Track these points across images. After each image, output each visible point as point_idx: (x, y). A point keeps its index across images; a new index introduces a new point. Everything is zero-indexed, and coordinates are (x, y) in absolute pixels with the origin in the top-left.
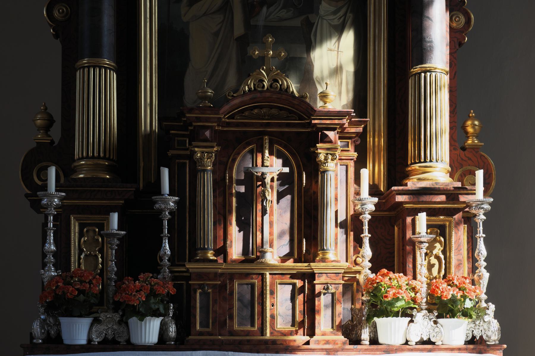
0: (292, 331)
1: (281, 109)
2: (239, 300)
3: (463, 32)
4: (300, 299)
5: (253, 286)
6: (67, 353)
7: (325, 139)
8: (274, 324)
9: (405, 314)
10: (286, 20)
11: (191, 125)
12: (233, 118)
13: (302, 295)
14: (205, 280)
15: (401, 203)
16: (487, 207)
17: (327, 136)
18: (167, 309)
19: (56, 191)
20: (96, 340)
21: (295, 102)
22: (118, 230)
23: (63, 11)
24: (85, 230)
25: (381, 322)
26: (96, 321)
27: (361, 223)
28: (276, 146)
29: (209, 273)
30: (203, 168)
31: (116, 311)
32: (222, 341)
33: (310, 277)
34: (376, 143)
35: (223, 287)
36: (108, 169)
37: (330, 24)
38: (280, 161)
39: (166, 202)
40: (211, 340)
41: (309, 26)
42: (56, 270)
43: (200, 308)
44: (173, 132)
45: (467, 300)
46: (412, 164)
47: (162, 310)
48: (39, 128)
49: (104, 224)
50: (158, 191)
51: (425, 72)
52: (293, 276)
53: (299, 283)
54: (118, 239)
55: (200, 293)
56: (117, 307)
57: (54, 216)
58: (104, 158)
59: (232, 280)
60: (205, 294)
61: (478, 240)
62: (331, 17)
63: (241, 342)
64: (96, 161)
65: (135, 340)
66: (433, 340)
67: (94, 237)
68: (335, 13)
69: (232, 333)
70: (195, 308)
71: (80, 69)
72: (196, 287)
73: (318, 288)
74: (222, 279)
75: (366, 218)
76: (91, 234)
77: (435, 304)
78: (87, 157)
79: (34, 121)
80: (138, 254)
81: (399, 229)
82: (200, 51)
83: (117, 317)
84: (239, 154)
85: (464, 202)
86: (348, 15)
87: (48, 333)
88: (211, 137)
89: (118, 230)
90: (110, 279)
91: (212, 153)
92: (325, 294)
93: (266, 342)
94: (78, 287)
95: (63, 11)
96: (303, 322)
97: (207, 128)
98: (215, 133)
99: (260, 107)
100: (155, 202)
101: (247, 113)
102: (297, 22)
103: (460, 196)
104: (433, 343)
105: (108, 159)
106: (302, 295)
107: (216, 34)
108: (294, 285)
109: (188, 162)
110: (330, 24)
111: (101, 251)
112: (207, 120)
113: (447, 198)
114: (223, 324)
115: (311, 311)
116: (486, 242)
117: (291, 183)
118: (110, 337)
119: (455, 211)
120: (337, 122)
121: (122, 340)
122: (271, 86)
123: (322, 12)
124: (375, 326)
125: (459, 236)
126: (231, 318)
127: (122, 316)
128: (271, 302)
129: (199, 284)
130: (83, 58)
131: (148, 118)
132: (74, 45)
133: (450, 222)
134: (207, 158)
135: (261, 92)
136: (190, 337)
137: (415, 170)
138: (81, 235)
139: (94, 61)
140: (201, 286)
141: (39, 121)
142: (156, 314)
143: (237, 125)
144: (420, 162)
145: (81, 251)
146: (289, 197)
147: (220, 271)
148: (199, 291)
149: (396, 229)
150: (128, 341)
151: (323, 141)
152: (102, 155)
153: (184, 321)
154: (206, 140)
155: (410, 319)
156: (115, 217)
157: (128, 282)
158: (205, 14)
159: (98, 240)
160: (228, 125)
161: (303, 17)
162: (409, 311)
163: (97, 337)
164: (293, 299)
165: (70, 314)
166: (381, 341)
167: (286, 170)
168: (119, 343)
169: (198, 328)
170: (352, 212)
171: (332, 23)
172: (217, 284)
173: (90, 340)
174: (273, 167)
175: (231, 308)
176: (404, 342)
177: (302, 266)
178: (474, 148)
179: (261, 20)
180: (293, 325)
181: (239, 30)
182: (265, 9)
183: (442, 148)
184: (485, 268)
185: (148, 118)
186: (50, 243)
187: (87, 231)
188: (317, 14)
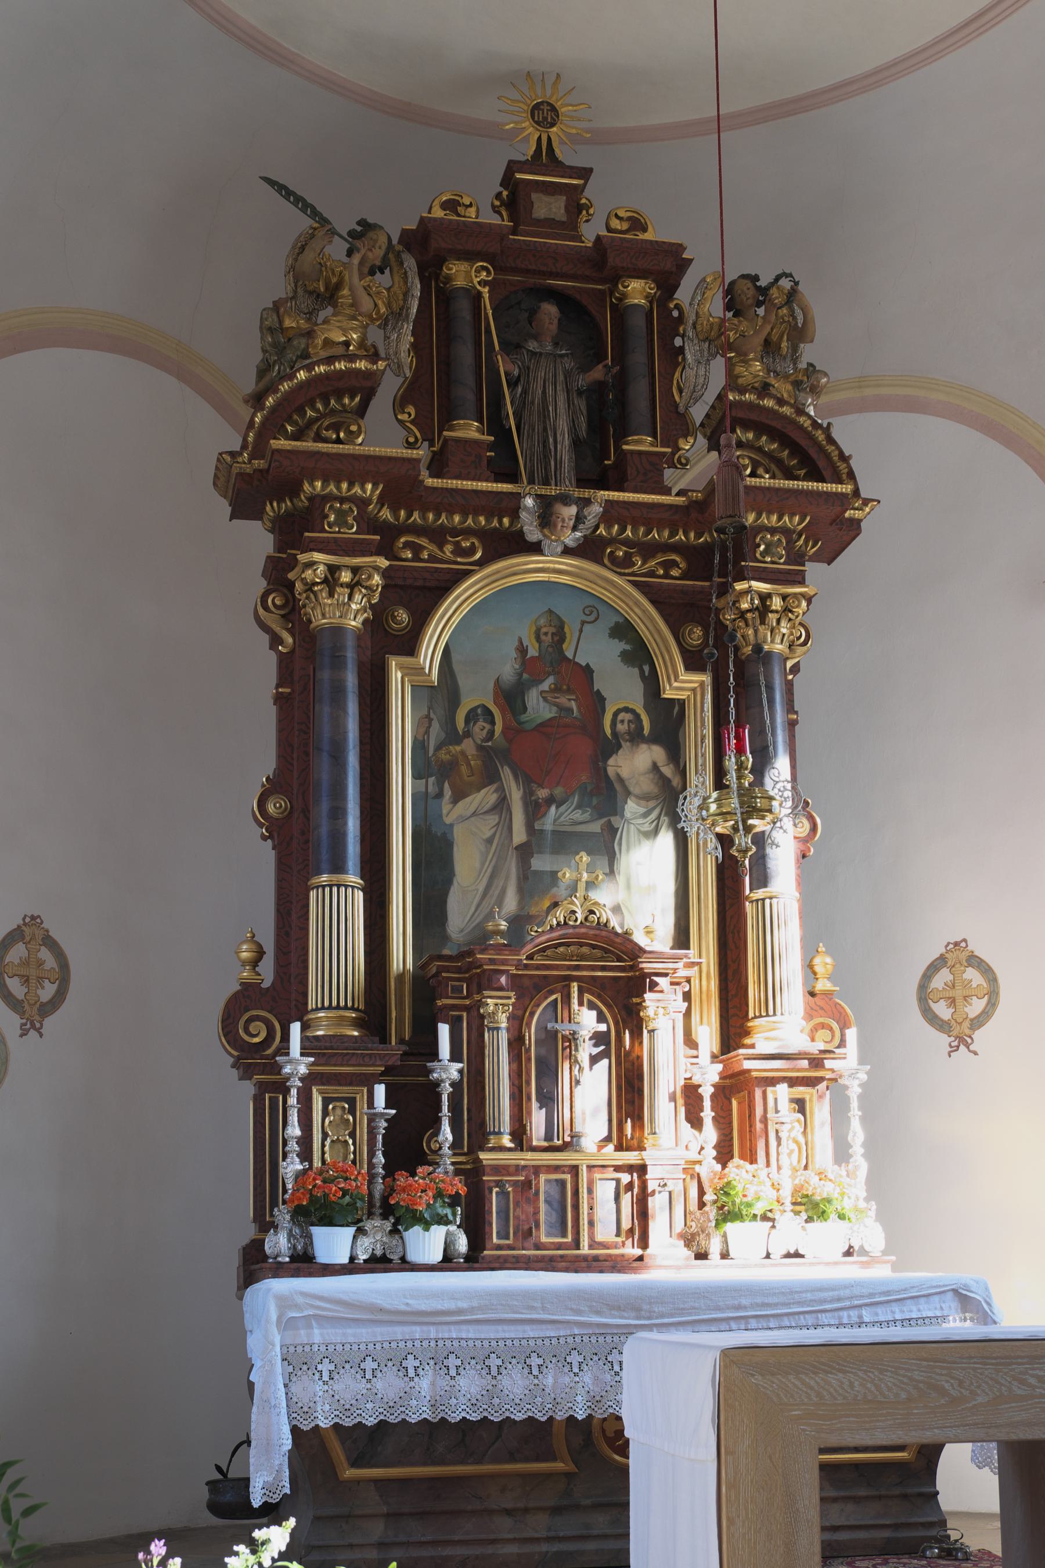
0: (617, 1243)
1: (594, 947)
2: (546, 1201)
3: (807, 842)
4: (626, 1199)
5: (562, 1183)
6: (324, 1276)
7: (653, 985)
8: (593, 1233)
9: (765, 1218)
10: (581, 823)
11: (480, 966)
12: (532, 959)
13: (630, 1193)
14: (503, 1175)
15: (749, 1071)
16: (863, 1077)
17: (657, 984)
18: (454, 1214)
19: (302, 1055)
20: (362, 1257)
21: (618, 940)
22: (386, 1108)
23: (281, 806)
24: (331, 1107)
25: (730, 1227)
26: (360, 1232)
27: (700, 1098)
28: (587, 996)
29: (509, 1166)
30: (495, 1025)
31: (385, 1217)
32: (529, 1257)
33: (641, 1169)
34: (704, 988)
35: (527, 1184)
36: (357, 1023)
37: (639, 830)
38: (594, 1014)
39: (445, 1069)
40: (514, 1256)
41: (612, 831)
42: (301, 1163)
43: (497, 1213)
44: (559, 1466)
45: (846, 1198)
46: (755, 1017)
47: (451, 1217)
48: (244, 963)
49: (355, 1098)
50: (434, 1055)
51: (771, 898)
52: (618, 1169)
53: (625, 1178)
54: (386, 1120)
55: (497, 1193)
56: (387, 1210)
57: (299, 1089)
58: (353, 1008)
59: (537, 1174)
60: (503, 1194)
61: (852, 1120)
62: (641, 821)
63: (552, 1259)
64: (342, 1013)
65: (413, 1257)
66: (801, 1252)
67: (342, 1116)
68: (645, 815)
69: (538, 1246)
70: (491, 1212)
71: (317, 887)
72: (493, 1184)
73: (652, 1186)
74: (524, 1174)
75: (707, 1092)
76: (339, 1112)
77: (800, 1204)
78: (330, 1007)
79: (237, 953)
80: (407, 1148)
81: (739, 1103)
82: (468, 864)
83: (388, 1225)
84: (538, 1005)
85: (833, 1070)
86: (662, 818)
87: (294, 1247)
88: (507, 984)
89: (386, 1108)
90: (377, 1174)
91: (508, 1005)
92: (660, 1192)
93: (585, 1258)
94: (342, 1185)
95: (281, 806)
96: (631, 1232)
97: (502, 972)
98: (513, 977)
99: (568, 945)
100: (431, 1071)
101: (549, 952)
102: (596, 827)
103: (825, 1061)
104: (802, 1256)
105: (357, 1010)
106: (630, 1193)
107: (489, 841)
108: (618, 1181)
109: (465, 1014)
110: (639, 830)
111: (353, 1135)
112: (504, 962)
113: (810, 1064)
114: (530, 1232)
115: (643, 1214)
116: (863, 1119)
117: (608, 1044)
118: (379, 1253)
119: (821, 1079)
120: (671, 966)
121: (395, 1257)
122: (586, 919)
123: (628, 814)
124: (725, 1236)
125: (821, 1112)
126: (538, 1226)
127: (395, 1225)
128: (589, 1203)
129: (495, 1181)
130: (319, 873)
131: (401, 955)
132: (299, 852)
133: (812, 1095)
134: (498, 1009)
135: (574, 927)
136: (485, 1252)
137: (760, 1026)
138: (325, 1113)
139: (335, 878)
140: (498, 1183)
141: (245, 954)
142: (443, 1221)
143: (538, 967)
144: (768, 1015)
145: (325, 1135)
146: (605, 1062)
147: (523, 1163)
148: (495, 1190)
149: (734, 1103)
150: (403, 1259)
151: (651, 990)
152: (349, 1004)
153: (475, 1228)
154: (501, 989)
155: (770, 1224)
156: (380, 1090)
157: (402, 1179)
158: (474, 814)
159: (348, 1120)
160: (526, 967)
161: (606, 819)
162: (769, 1215)
163: (364, 1254)
164: (617, 1198)
165: (331, 1223)
166: (732, 1254)
167: (603, 1027)
168: (390, 1261)
169: (495, 1240)
170: (682, 1082)
171: (642, 829)
172: (518, 1181)
173: (352, 1259)
174: (588, 1021)
175: (536, 1212)
176: (764, 1254)
177: (631, 1157)
178: (828, 994)
179: (549, 821)
180: (618, 1235)
181: (519, 836)
182: (553, 808)
183: (793, 999)
184: (862, 1155)
185: (401, 955)
186: (293, 1126)
187: (344, 1108)
188: (622, 816)
